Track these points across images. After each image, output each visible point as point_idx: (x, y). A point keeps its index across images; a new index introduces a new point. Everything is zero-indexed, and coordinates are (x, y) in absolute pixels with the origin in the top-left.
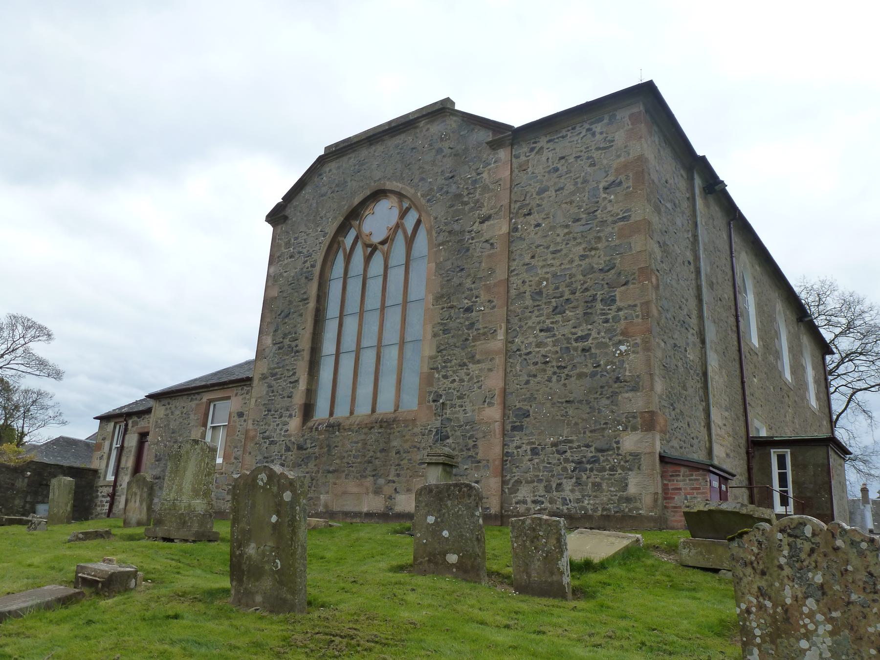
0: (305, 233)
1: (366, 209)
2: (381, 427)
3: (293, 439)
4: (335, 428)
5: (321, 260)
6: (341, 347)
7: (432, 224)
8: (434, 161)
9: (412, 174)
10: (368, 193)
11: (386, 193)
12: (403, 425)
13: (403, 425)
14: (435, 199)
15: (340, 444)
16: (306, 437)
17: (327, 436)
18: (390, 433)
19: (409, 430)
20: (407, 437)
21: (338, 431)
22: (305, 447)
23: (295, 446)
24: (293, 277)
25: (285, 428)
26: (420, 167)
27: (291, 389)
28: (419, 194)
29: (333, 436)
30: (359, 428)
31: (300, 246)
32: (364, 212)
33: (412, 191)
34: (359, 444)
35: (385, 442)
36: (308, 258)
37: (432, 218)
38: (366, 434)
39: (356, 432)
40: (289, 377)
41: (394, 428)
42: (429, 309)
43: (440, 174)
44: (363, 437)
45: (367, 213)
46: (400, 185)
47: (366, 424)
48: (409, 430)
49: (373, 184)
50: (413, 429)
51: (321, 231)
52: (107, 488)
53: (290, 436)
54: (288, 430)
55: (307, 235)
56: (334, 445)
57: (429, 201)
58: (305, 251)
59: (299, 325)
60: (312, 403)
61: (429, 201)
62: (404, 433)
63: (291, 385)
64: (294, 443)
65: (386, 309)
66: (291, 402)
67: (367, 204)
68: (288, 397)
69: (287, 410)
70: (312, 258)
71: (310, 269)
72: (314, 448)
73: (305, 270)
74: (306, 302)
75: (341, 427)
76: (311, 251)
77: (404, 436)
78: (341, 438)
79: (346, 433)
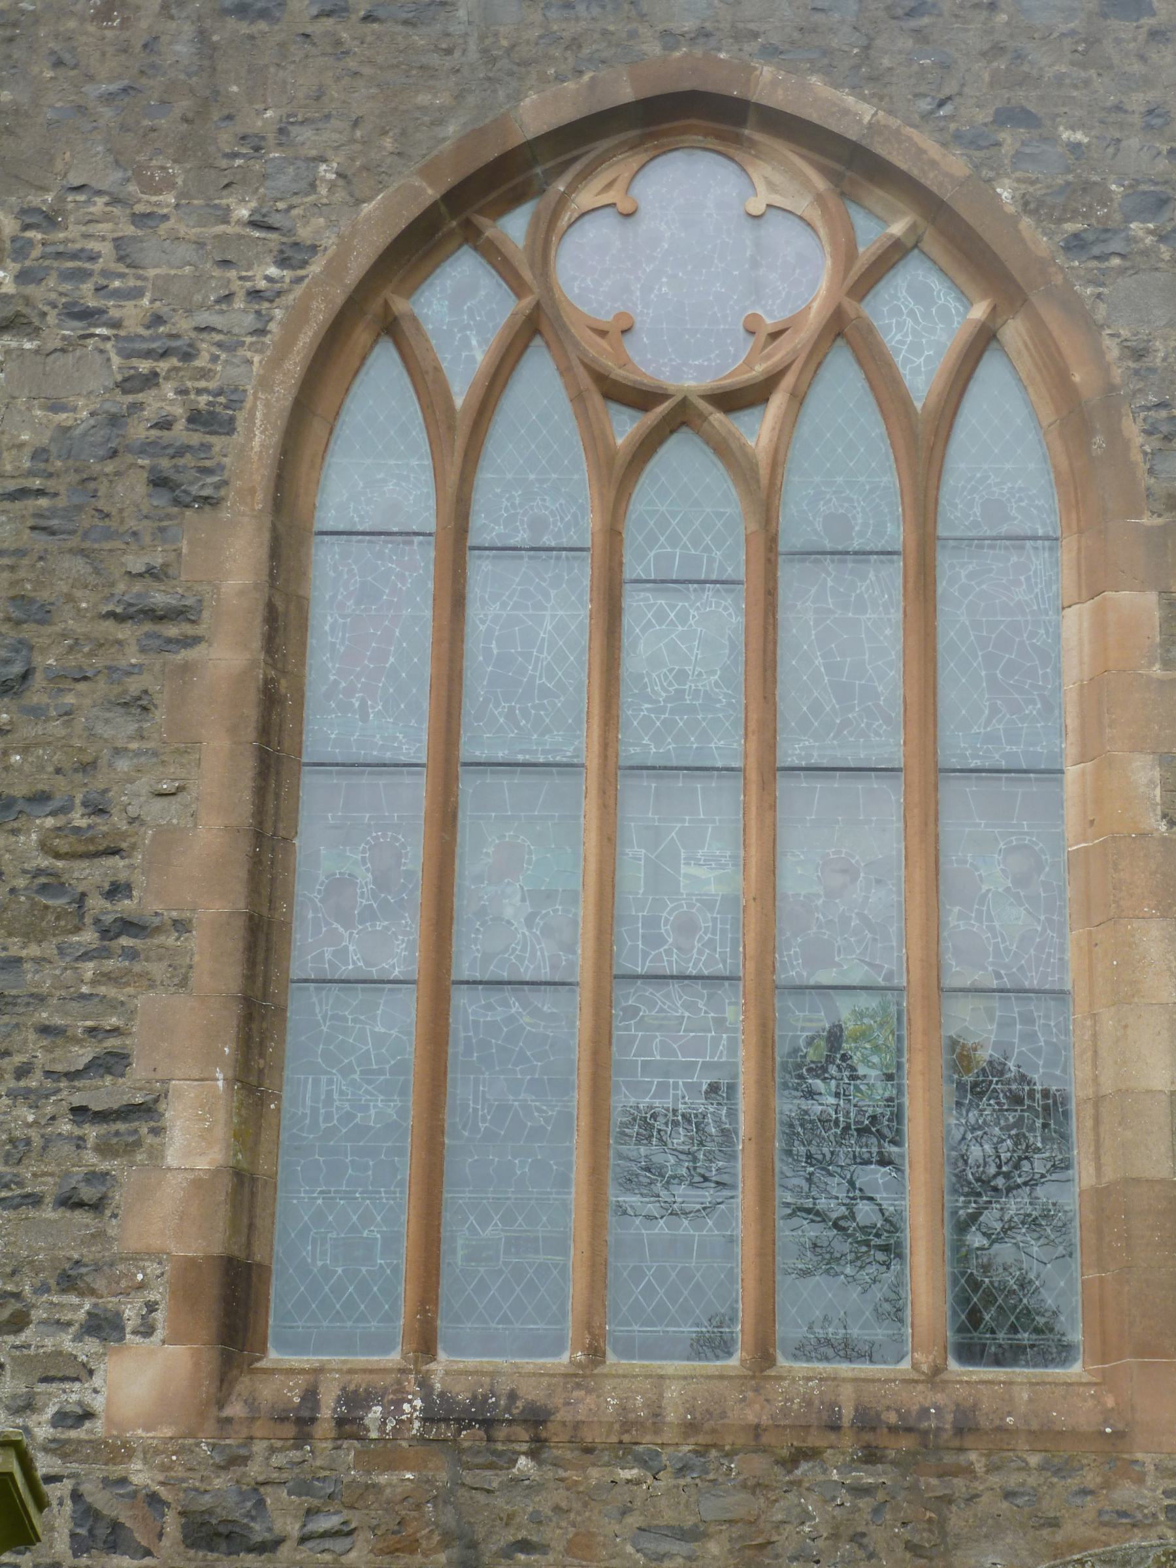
0: (115, 201)
1: (585, 175)
2: (871, 1456)
3: (140, 1474)
4: (502, 1432)
5: (283, 393)
6: (458, 945)
7: (1117, 374)
8: (1092, 41)
9: (945, 67)
10: (626, 93)
11: (741, 121)
12: (1034, 1460)
13: (1034, 1460)
14: (1117, 245)
15: (555, 1534)
16: (255, 1470)
17: (443, 1477)
18: (948, 1500)
19: (1085, 1492)
20: (1070, 1530)
21: (532, 1454)
22: (258, 1532)
23: (172, 1525)
24: (40, 454)
25: (73, 1395)
26: (998, 50)
27: (91, 1158)
28: (1005, 194)
29: (494, 1480)
30: (701, 1451)
31: (85, 275)
32: (572, 188)
33: (956, 164)
34: (713, 1548)
35: (910, 1546)
36: (163, 366)
37: (1113, 351)
38: (757, 1487)
39: (682, 1471)
40: (71, 1076)
41: (968, 1471)
42: (1143, 835)
43: (1136, 119)
44: (737, 1503)
45: (586, 198)
46: (867, 112)
47: (757, 1430)
48: (1085, 1492)
49: (653, 48)
50: (1107, 1485)
51: (254, 224)
52: (321, 1530)
53: (119, 1451)
54: (88, 1415)
55: (140, 219)
56: (510, 1536)
57: (1076, 244)
58: (132, 314)
59: (123, 765)
60: (258, 1258)
61: (1076, 244)
62: (1049, 1507)
63: (92, 1132)
64: (153, 1499)
65: (783, 783)
66: (100, 1236)
67: (603, 145)
68: (70, 1202)
69: (69, 1281)
70: (204, 374)
71: (180, 433)
72: (339, 1544)
73: (139, 431)
74: (172, 631)
75: (551, 1431)
76: (183, 324)
77: (1054, 1523)
78: (560, 1496)
79: (594, 1473)
